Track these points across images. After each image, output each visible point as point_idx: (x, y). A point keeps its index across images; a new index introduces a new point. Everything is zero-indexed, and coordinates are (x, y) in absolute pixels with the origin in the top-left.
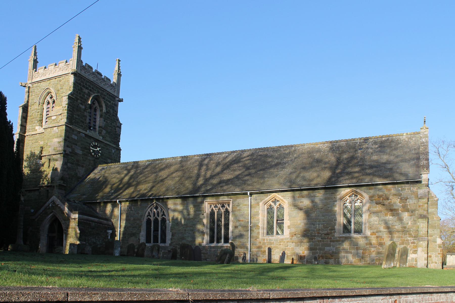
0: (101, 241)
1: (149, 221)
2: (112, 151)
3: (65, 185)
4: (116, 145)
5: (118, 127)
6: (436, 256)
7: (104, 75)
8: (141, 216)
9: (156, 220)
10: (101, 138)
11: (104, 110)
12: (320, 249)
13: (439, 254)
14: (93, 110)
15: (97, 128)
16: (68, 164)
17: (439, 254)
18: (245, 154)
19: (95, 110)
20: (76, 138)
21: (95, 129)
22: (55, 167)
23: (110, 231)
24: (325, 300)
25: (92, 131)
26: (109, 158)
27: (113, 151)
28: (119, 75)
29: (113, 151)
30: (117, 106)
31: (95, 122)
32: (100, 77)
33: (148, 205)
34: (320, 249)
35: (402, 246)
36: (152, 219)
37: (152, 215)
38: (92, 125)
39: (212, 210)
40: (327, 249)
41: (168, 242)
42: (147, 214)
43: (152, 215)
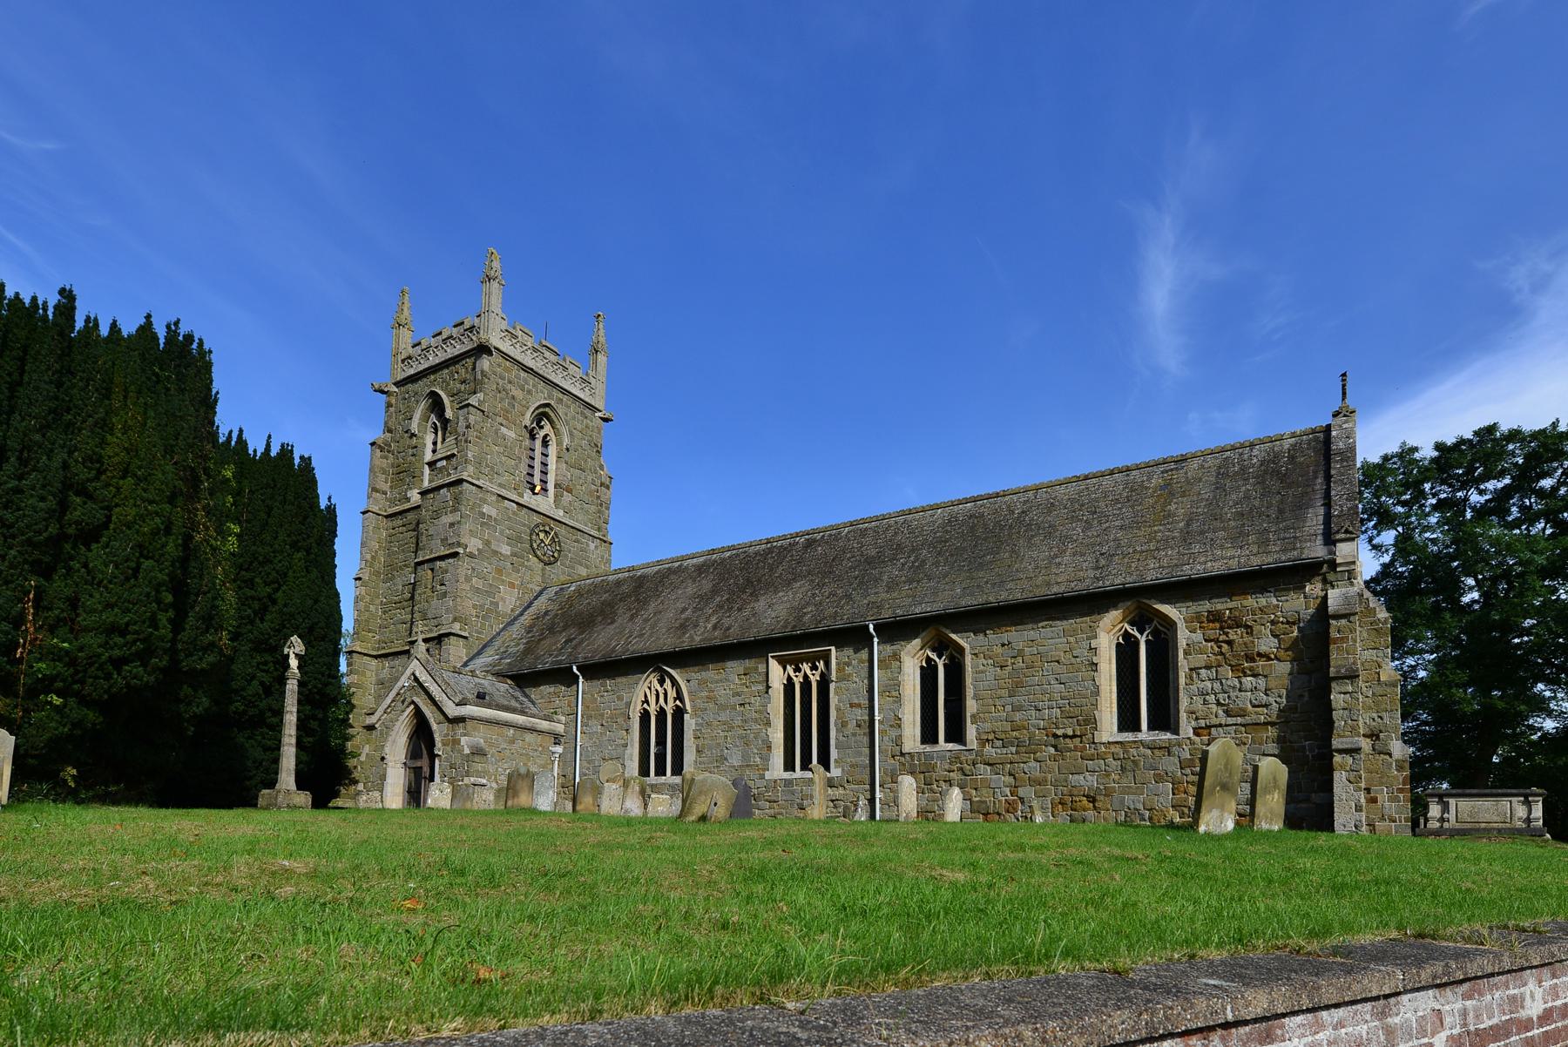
1: (645, 716)
6: (1393, 799)
7: (1469, 435)
8: (628, 704)
9: (662, 714)
10: (561, 513)
13: (1401, 791)
14: (538, 443)
17: (1401, 791)
19: (545, 443)
20: (493, 513)
21: (545, 490)
22: (183, 329)
24: (1216, 1042)
25: (539, 497)
27: (592, 546)
29: (592, 546)
37: (652, 700)
38: (537, 480)
39: (789, 679)
43: (652, 700)
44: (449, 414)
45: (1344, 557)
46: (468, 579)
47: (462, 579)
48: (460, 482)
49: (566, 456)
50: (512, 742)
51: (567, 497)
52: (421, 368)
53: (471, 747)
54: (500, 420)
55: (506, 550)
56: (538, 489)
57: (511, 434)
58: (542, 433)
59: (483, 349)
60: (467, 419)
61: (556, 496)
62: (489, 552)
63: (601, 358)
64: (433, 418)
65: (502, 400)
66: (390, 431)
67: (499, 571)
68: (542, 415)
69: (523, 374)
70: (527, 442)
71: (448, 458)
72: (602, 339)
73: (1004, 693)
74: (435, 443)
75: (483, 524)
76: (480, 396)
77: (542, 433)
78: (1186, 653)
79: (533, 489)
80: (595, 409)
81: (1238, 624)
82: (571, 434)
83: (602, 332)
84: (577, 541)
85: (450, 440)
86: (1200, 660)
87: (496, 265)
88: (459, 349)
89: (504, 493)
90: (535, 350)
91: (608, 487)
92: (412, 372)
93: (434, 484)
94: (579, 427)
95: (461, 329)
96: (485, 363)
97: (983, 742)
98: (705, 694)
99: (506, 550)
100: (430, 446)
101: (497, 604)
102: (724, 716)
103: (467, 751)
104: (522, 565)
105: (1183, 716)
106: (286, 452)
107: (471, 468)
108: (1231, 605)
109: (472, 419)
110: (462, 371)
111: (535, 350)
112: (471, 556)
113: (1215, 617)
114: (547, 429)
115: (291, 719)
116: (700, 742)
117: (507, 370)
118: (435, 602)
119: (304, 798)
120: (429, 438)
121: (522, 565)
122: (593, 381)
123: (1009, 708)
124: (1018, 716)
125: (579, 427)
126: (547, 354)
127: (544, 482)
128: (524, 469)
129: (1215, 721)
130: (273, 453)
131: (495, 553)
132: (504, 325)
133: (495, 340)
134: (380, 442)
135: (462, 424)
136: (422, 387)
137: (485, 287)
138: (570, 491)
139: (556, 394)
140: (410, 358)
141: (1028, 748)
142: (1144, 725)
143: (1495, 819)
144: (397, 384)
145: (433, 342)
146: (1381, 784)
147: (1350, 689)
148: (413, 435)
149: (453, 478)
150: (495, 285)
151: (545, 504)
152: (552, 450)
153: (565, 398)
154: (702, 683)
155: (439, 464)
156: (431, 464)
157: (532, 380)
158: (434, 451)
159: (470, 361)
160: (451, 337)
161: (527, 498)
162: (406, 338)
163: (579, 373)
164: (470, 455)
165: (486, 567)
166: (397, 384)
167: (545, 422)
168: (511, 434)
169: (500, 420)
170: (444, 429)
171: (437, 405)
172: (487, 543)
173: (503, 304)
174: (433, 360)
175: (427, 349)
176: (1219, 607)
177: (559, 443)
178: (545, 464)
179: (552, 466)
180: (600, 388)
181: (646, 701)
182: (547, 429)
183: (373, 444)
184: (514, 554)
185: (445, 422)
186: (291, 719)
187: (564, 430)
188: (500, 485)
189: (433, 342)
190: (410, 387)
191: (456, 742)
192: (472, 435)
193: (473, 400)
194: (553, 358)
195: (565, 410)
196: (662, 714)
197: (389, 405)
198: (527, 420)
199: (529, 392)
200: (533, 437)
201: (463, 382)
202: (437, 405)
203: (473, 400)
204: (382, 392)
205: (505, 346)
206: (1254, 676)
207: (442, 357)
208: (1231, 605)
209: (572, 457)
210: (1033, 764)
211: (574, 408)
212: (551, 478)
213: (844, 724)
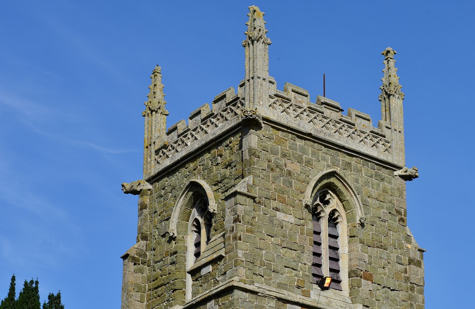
5: (411, 262)
11: (359, 214)
14: (324, 223)
15: (344, 275)
19: (333, 221)
21: (337, 281)
31: (334, 260)
38: (325, 271)
44: (213, 206)
48: (230, 290)
49: (361, 233)
51: (366, 285)
52: (178, 156)
54: (274, 204)
56: (328, 281)
58: (328, 209)
59: (250, 123)
60: (234, 211)
61: (352, 287)
63: (396, 103)
64: (195, 213)
66: (144, 238)
69: (299, 143)
70: (310, 225)
71: (214, 262)
72: (395, 80)
74: (198, 245)
76: (249, 179)
77: (328, 209)
79: (321, 284)
80: (392, 167)
81: (231, 163)
82: (365, 205)
83: (393, 71)
85: (216, 237)
87: (260, 23)
88: (222, 127)
89: (286, 294)
90: (312, 110)
91: (419, 264)
92: (167, 163)
93: (199, 297)
94: (374, 193)
95: (222, 104)
96: (253, 139)
100: (192, 249)
106: (31, 290)
107: (242, 271)
109: (240, 208)
110: (225, 153)
111: (312, 110)
114: (335, 203)
117: (280, 142)
120: (191, 239)
122: (387, 132)
125: (374, 193)
126: (327, 112)
127: (335, 271)
128: (308, 259)
130: (196, 229)
132: (273, 90)
133: (264, 110)
134: (133, 253)
135: (229, 217)
136: (180, 179)
137: (248, 51)
138: (369, 277)
139: (342, 158)
140: (165, 147)
144: (151, 180)
145: (191, 124)
148: (172, 238)
149: (221, 286)
150: (259, 46)
152: (343, 229)
153: (353, 161)
155: (204, 271)
156: (194, 272)
157: (310, 147)
158: (197, 255)
159: (235, 140)
160: (211, 115)
162: (160, 123)
163: (368, 127)
164: (240, 254)
166: (151, 180)
167: (331, 196)
168: (291, 219)
169: (274, 204)
170: (209, 226)
171: (198, 198)
173: (270, 65)
175: (184, 134)
177: (350, 219)
178: (334, 249)
179: (343, 243)
180: (397, 139)
182: (335, 203)
183: (125, 257)
185: (209, 217)
187: (355, 202)
188: (280, 286)
189: (191, 124)
190: (166, 181)
192: (241, 228)
193: (241, 187)
194: (335, 115)
195: (355, 175)
197: (143, 207)
198: (308, 198)
199: (308, 163)
200: (316, 216)
201: (228, 165)
202: (198, 198)
203: (241, 187)
204: (135, 192)
205: (276, 114)
207: (202, 139)
209: (368, 233)
211: (367, 170)
212: (344, 267)
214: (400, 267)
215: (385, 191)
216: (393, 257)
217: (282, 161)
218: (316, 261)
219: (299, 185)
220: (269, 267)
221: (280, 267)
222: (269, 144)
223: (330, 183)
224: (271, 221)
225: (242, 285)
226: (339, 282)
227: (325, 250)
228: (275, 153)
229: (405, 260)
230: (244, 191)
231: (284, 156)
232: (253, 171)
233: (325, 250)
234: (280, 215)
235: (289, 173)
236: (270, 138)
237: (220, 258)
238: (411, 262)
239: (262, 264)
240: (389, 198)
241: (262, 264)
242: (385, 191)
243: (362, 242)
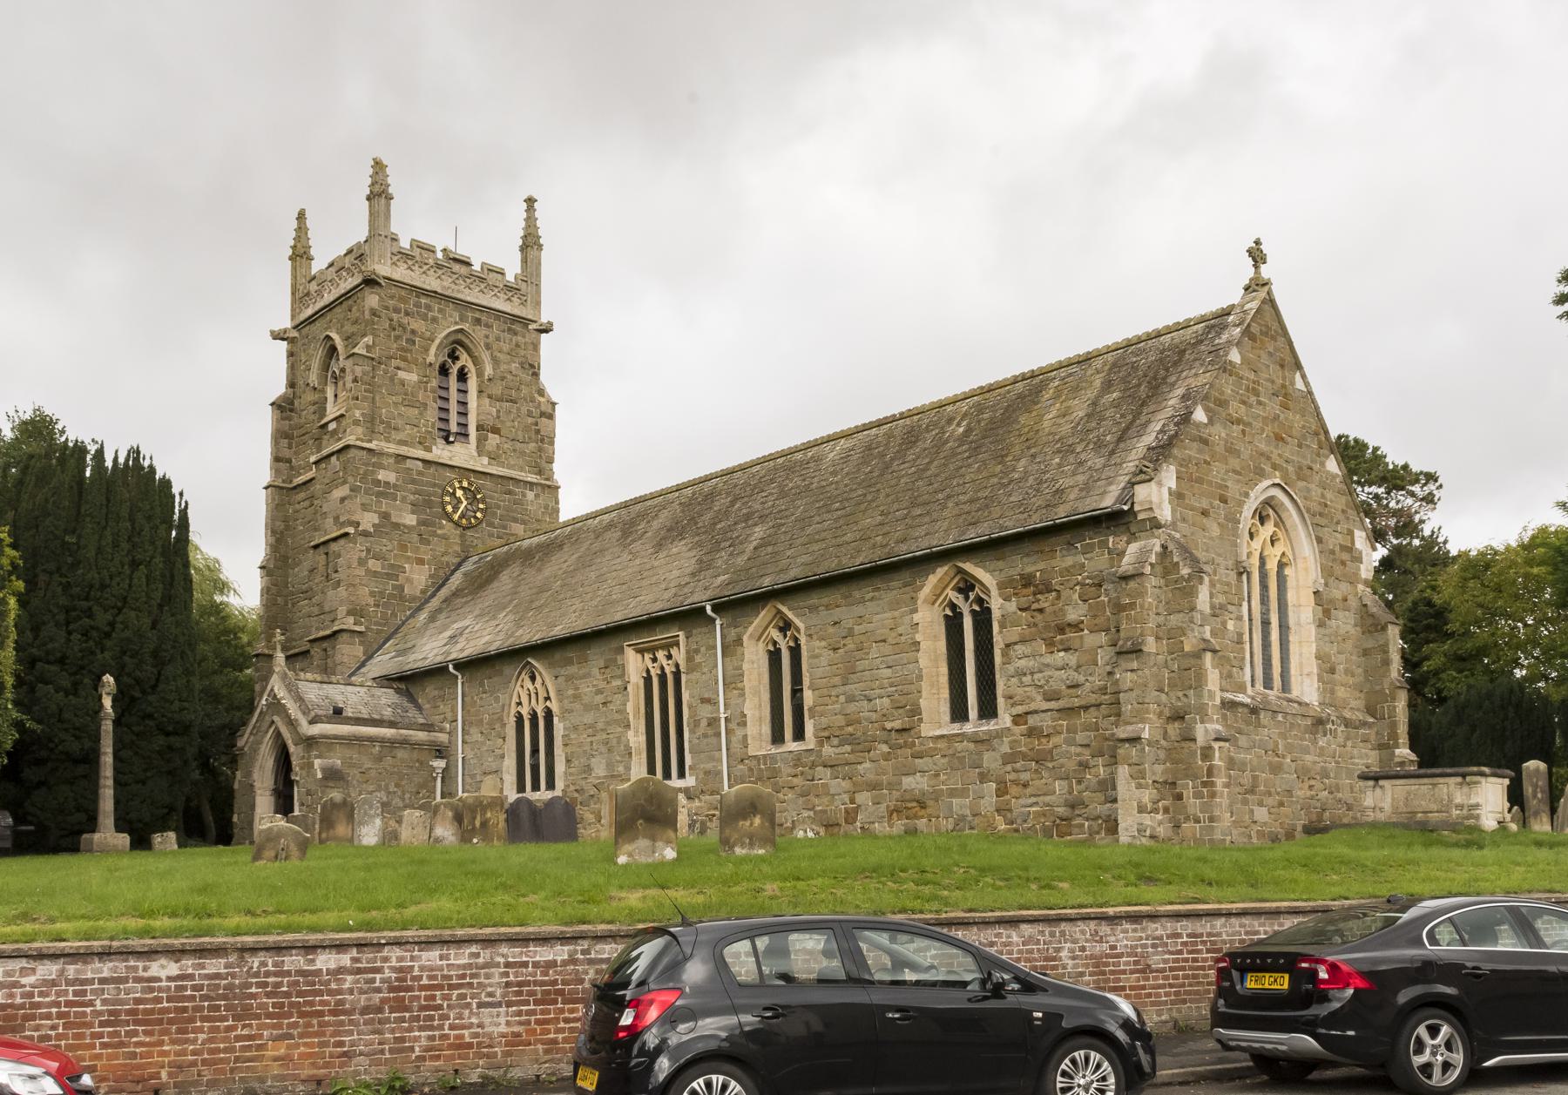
0: (407, 796)
1: (520, 718)
2: (524, 495)
3: (362, 629)
4: (540, 473)
5: (543, 414)
9: (534, 717)
10: (485, 460)
11: (489, 370)
12: (891, 786)
15: (472, 430)
16: (371, 562)
18: (832, 453)
19: (462, 376)
23: (440, 764)
26: (515, 520)
28: (530, 243)
30: (536, 347)
31: (464, 414)
32: (463, 270)
33: (276, 706)
34: (891, 786)
35: (683, 819)
36: (525, 711)
37: (525, 700)
38: (454, 428)
40: (908, 782)
41: (560, 784)
42: (515, 699)
43: (525, 700)
45: (1141, 503)
46: (362, 562)
47: (355, 564)
48: (347, 447)
50: (379, 759)
51: (493, 440)
53: (323, 770)
55: (410, 520)
57: (411, 377)
58: (459, 364)
59: (370, 282)
62: (387, 524)
65: (397, 338)
67: (403, 547)
68: (456, 345)
73: (837, 680)
75: (379, 494)
78: (1002, 626)
82: (496, 361)
84: (510, 492)
86: (1014, 633)
89: (404, 450)
97: (821, 741)
98: (570, 692)
99: (410, 520)
101: (402, 588)
102: (588, 718)
103: (319, 776)
104: (434, 534)
105: (1001, 701)
108: (1041, 565)
112: (365, 534)
113: (1027, 581)
115: (108, 759)
116: (569, 750)
118: (331, 593)
119: (124, 839)
121: (434, 534)
123: (842, 699)
124: (852, 708)
125: (506, 347)
129: (1033, 706)
131: (397, 526)
136: (317, 329)
138: (496, 431)
141: (862, 745)
142: (973, 712)
143: (1434, 807)
146: (1187, 777)
147: (1135, 665)
149: (340, 445)
151: (462, 454)
152: (472, 384)
154: (569, 678)
161: (440, 452)
165: (386, 545)
169: (394, 363)
172: (385, 516)
174: (328, 298)
176: (1029, 569)
177: (480, 374)
181: (519, 704)
184: (421, 523)
186: (108, 759)
187: (485, 357)
191: (311, 765)
196: (534, 717)
199: (434, 320)
206: (1066, 650)
208: (1041, 565)
210: (867, 765)
213: (696, 723)
214: (530, 420)
215: (517, 345)
216: (524, 410)
217: (405, 320)
218: (443, 416)
219: (424, 343)
220: (389, 425)
221: (400, 422)
222: (391, 302)
223: (16, 626)
224: (392, 379)
225: (359, 443)
226: (466, 435)
227: (453, 407)
228: (397, 311)
229: (536, 412)
230: (364, 352)
231: (407, 314)
232: (516, 1029)
233: (453, 407)
234: (402, 374)
235: (413, 332)
236: (392, 297)
237: (342, 416)
238: (543, 414)
239: (382, 422)
240: (522, 353)
241: (382, 422)
242: (517, 345)
243: (490, 397)
